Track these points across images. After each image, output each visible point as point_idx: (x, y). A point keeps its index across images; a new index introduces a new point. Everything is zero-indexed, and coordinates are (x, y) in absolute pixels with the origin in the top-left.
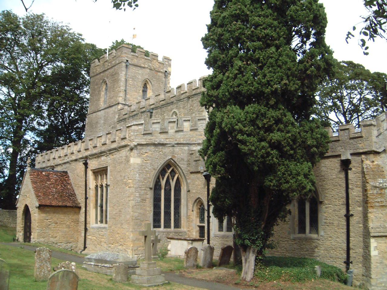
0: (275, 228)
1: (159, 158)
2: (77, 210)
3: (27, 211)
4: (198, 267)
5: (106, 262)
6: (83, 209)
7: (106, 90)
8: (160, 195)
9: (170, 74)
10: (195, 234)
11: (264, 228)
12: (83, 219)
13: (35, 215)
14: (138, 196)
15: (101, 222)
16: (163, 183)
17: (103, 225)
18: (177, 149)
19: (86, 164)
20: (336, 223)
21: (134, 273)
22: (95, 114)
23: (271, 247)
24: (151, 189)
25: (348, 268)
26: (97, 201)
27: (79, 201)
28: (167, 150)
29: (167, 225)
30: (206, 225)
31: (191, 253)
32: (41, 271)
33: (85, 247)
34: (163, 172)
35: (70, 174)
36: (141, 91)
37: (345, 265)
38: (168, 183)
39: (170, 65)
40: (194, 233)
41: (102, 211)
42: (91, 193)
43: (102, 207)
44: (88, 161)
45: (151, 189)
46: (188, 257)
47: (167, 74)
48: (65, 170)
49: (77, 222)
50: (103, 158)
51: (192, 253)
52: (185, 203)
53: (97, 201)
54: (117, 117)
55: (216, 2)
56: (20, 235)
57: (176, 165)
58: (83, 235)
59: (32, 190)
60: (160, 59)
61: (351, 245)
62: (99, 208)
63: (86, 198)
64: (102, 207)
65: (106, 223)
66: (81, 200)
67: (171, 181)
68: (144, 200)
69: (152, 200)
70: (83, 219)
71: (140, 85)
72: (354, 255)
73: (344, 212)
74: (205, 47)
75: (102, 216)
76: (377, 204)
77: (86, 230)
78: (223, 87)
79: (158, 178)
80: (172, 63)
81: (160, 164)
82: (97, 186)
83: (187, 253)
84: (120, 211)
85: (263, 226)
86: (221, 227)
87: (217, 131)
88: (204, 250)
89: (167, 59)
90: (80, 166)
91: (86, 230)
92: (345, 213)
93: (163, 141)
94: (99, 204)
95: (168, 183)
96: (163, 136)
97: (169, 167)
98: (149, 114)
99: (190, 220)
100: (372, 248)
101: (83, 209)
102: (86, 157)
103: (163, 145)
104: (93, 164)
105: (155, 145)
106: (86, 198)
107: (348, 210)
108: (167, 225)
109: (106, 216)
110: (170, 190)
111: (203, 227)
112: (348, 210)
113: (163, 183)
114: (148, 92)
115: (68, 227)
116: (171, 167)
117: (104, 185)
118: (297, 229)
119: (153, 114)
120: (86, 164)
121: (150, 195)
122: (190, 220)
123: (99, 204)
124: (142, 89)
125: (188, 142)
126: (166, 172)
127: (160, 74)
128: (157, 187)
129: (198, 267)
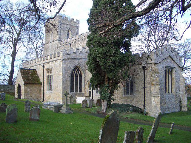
0: (115, 92)
1: (73, 64)
2: (40, 85)
3: (19, 86)
4: (87, 107)
5: (51, 105)
6: (43, 85)
7: (52, 34)
8: (73, 79)
9: (79, 27)
10: (87, 94)
11: (110, 92)
12: (42, 89)
13: (23, 87)
14: (169, 22)
15: (50, 90)
16: (74, 74)
17: (51, 91)
18: (80, 61)
19: (44, 66)
20: (140, 91)
21: (61, 109)
22: (47, 44)
23: (113, 99)
24: (70, 76)
25: (144, 108)
26: (48, 81)
27: (41, 81)
28: (76, 61)
29: (76, 91)
30: (91, 91)
31: (85, 102)
32: (27, 109)
33: (44, 100)
34: (74, 70)
35: (37, 71)
36: (67, 35)
37: (143, 107)
38: (76, 74)
39: (79, 23)
40: (87, 94)
41: (50, 85)
42: (46, 78)
43: (50, 84)
44: (45, 65)
45: (70, 76)
46: (83, 103)
47: (78, 27)
48: (35, 69)
49: (40, 90)
50: (50, 64)
51: (85, 102)
52: (84, 82)
53: (48, 81)
54: (57, 46)
55: (94, 2)
56: (16, 96)
57: (80, 67)
58: (43, 95)
59: (22, 77)
60: (75, 21)
61: (145, 99)
62: (49, 84)
63: (44, 80)
64: (50, 84)
65: (52, 90)
66: (42, 81)
67: (78, 73)
68: (67, 81)
69: (70, 81)
70: (43, 89)
71: (66, 32)
72: (147, 103)
73: (143, 86)
74: (88, 24)
75: (50, 88)
76: (155, 84)
77: (44, 93)
78: (94, 40)
79: (73, 72)
80: (80, 22)
81: (73, 67)
82: (48, 75)
83: (83, 102)
84: (57, 86)
85: (110, 92)
86: (72, 91)
87: (92, 57)
88: (90, 101)
89: (78, 21)
90: (41, 67)
91: (44, 93)
92: (144, 87)
93: (74, 57)
94: (49, 83)
95: (76, 74)
96: (74, 55)
97: (76, 69)
98: (70, 45)
99: (86, 88)
100: (153, 101)
101: (43, 85)
102: (44, 63)
103: (75, 59)
104: (47, 66)
105: (71, 59)
106: (44, 80)
107: (144, 86)
108: (76, 91)
109: (52, 87)
110: (78, 77)
111: (91, 91)
112: (144, 86)
113: (74, 74)
114: (70, 35)
115: (37, 92)
116: (77, 68)
117: (51, 75)
118: (126, 93)
119: (71, 45)
120: (44, 66)
121: (69, 79)
122: (86, 88)
123: (49, 83)
124: (67, 34)
125: (84, 57)
126: (76, 70)
127: (75, 27)
128: (72, 76)
129: (87, 107)
